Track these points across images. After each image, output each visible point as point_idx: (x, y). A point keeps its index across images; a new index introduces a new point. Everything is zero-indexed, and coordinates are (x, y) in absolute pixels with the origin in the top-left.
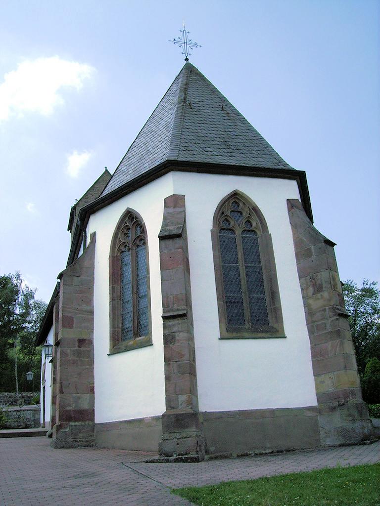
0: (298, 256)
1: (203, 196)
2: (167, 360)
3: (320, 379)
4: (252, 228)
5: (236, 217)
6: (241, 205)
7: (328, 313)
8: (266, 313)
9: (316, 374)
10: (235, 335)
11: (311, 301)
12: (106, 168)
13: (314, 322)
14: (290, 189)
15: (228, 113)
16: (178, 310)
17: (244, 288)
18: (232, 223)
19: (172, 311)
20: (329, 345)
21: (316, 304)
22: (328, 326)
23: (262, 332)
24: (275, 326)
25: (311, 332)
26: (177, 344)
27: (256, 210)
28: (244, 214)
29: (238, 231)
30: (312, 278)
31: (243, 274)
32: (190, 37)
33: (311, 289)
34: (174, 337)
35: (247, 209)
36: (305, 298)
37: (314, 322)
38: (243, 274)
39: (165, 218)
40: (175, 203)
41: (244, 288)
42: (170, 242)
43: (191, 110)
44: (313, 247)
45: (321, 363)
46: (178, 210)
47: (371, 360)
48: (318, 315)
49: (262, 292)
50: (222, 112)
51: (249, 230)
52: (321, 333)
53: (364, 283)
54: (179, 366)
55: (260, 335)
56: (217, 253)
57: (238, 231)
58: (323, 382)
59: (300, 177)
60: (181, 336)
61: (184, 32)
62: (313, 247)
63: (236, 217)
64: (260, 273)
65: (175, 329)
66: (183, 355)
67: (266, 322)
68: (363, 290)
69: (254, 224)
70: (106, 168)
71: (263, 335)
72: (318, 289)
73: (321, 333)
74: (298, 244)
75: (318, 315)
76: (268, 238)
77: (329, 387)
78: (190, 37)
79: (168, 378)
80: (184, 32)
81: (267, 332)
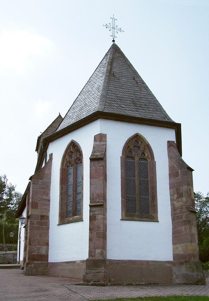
0: (171, 175)
1: (118, 135)
4: (145, 157)
5: (136, 150)
9: (174, 243)
10: (129, 218)
11: (175, 202)
12: (59, 113)
13: (176, 214)
14: (171, 135)
15: (137, 82)
16: (99, 202)
19: (95, 202)
20: (183, 228)
21: (177, 204)
22: (184, 217)
23: (145, 218)
25: (173, 220)
26: (97, 221)
28: (141, 148)
29: (137, 159)
30: (177, 189)
33: (176, 196)
35: (143, 146)
36: (172, 200)
37: (176, 214)
39: (94, 148)
40: (101, 138)
44: (180, 171)
46: (102, 143)
48: (178, 211)
54: (97, 234)
55: (144, 219)
57: (137, 159)
60: (99, 217)
62: (180, 171)
63: (136, 150)
65: (96, 213)
66: (100, 228)
69: (146, 155)
70: (59, 113)
71: (146, 219)
74: (171, 168)
75: (178, 211)
77: (180, 251)
78: (117, 23)
79: (90, 240)
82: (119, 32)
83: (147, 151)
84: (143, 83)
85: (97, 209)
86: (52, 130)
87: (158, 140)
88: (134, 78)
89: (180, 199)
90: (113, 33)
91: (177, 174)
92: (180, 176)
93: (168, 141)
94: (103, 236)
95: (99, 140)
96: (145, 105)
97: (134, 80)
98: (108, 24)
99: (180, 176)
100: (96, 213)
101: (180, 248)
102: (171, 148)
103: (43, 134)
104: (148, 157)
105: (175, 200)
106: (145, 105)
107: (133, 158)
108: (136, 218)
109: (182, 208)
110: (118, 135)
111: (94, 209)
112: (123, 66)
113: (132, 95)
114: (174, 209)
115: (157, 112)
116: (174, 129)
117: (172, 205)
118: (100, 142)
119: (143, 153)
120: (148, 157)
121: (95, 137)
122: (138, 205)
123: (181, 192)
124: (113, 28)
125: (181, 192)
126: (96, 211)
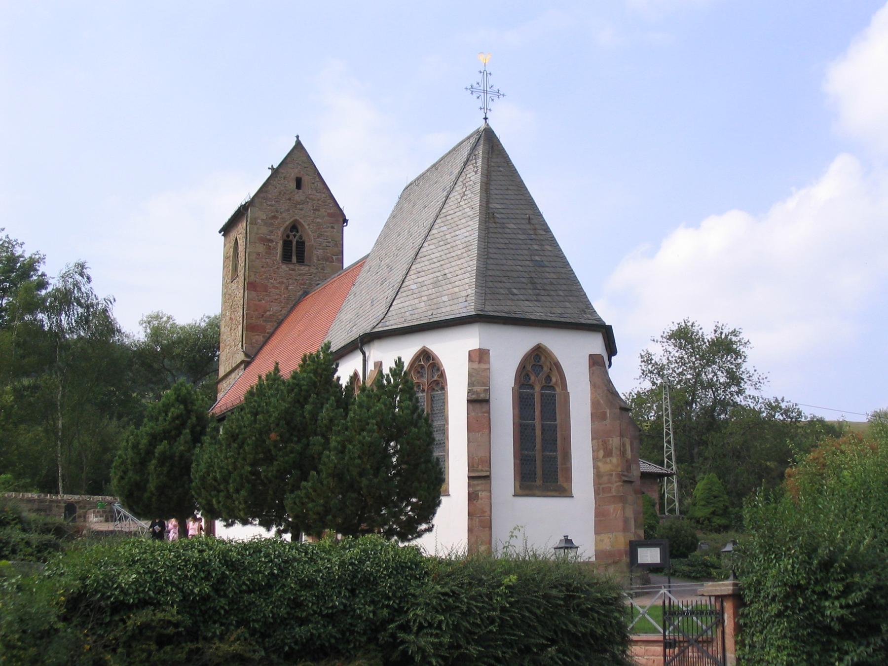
0: (593, 416)
1: (509, 349)
2: (470, 514)
3: (599, 538)
4: (551, 384)
5: (538, 371)
6: (543, 358)
7: (614, 478)
8: (556, 472)
9: (597, 532)
10: (527, 492)
11: (600, 464)
12: (298, 137)
13: (600, 484)
14: (595, 344)
15: (535, 229)
16: (482, 471)
17: (538, 446)
18: (533, 378)
19: (477, 471)
20: (611, 508)
21: (604, 468)
22: (613, 490)
23: (552, 491)
24: (565, 485)
25: (597, 493)
26: (480, 501)
27: (558, 366)
28: (545, 369)
29: (537, 388)
30: (605, 442)
31: (538, 432)
32: (492, 80)
33: (601, 453)
34: (477, 495)
35: (548, 364)
36: (595, 459)
37: (600, 484)
38: (538, 432)
39: (470, 375)
40: (479, 357)
41: (538, 446)
42: (478, 406)
43: (494, 225)
44: (608, 411)
45: (602, 523)
46: (483, 366)
47: (706, 477)
48: (605, 479)
49: (556, 451)
50: (528, 226)
51: (548, 385)
52: (606, 495)
53: (716, 331)
54: (480, 521)
55: (549, 493)
56: (517, 411)
57: (537, 388)
58: (602, 541)
59: (607, 333)
60: (482, 495)
61: (485, 74)
62: (608, 411)
63: (538, 371)
64: (555, 430)
65: (479, 488)
66: (484, 512)
67: (556, 480)
68: (713, 343)
69: (554, 380)
70: (298, 137)
71: (552, 493)
72: (608, 454)
73: (606, 495)
74: (595, 404)
75: (605, 479)
76: (567, 396)
77: (607, 546)
78: (492, 80)
79: (470, 530)
80: (485, 74)
81: (556, 491)
82: (496, 98)
83: (555, 372)
84: (547, 230)
85: (480, 482)
86: (278, 186)
87: (572, 353)
88: (529, 219)
89: (608, 460)
90: (485, 102)
91: (603, 417)
92: (608, 421)
93: (590, 355)
94: (487, 525)
95: (477, 359)
96: (552, 284)
97: (529, 223)
98: (475, 85)
99: (608, 421)
100: (479, 488)
101: (607, 541)
102: (594, 368)
103: (256, 200)
104: (556, 383)
105: (600, 460)
106: (552, 284)
107: (532, 387)
108: (537, 492)
109: (611, 475)
110: (509, 349)
111: (475, 482)
112: (508, 189)
113: (528, 263)
114: (598, 475)
115: (571, 298)
116: (599, 331)
117: (596, 467)
118: (479, 362)
119: (548, 378)
120: (556, 383)
121: (471, 354)
122: (541, 470)
123: (610, 447)
124: (485, 92)
125: (610, 447)
126: (478, 485)
